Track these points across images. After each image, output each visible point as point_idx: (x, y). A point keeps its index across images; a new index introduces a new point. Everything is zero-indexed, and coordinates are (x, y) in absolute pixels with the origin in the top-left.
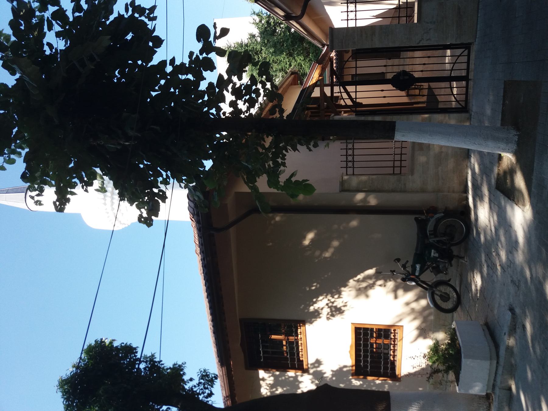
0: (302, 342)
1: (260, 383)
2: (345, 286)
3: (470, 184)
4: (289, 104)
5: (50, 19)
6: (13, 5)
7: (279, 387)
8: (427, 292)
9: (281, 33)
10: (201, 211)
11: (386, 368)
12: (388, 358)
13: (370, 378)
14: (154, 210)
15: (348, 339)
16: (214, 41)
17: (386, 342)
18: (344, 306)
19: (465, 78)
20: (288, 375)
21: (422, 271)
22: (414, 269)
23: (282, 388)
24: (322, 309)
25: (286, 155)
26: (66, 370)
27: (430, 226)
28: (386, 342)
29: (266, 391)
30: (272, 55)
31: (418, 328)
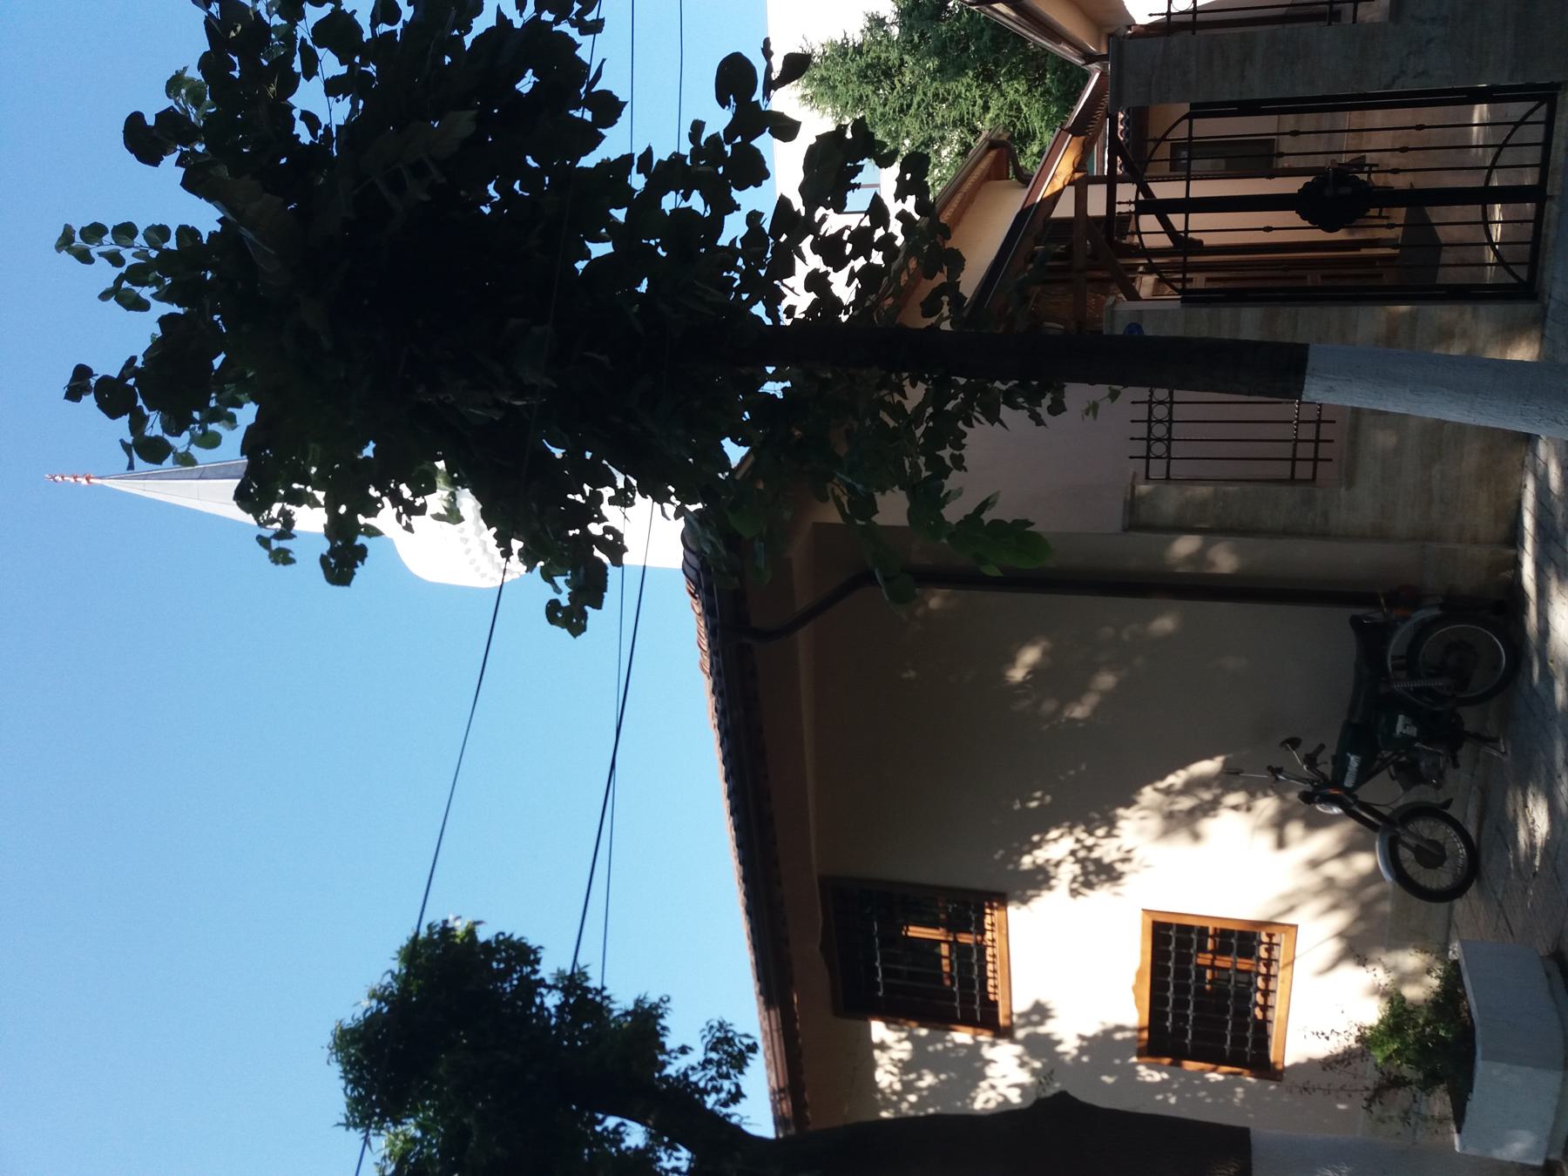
0: (996, 951)
1: (872, 1056)
2: (1129, 803)
3: (1528, 521)
4: (983, 241)
5: (309, 42)
6: (210, 14)
7: (925, 1071)
8: (1377, 836)
9: (961, 12)
10: (716, 574)
11: (1239, 1040)
12: (1248, 1012)
13: (1190, 1065)
14: (590, 589)
15: (1129, 957)
16: (767, 95)
17: (1244, 964)
18: (1124, 860)
19: (1535, 193)
20: (952, 1041)
21: (1365, 775)
22: (1340, 764)
23: (936, 1074)
24: (1058, 864)
25: (964, 435)
26: (354, 1006)
27: (1397, 645)
28: (1244, 964)
29: (889, 1078)
30: (933, 80)
31: (1341, 935)
